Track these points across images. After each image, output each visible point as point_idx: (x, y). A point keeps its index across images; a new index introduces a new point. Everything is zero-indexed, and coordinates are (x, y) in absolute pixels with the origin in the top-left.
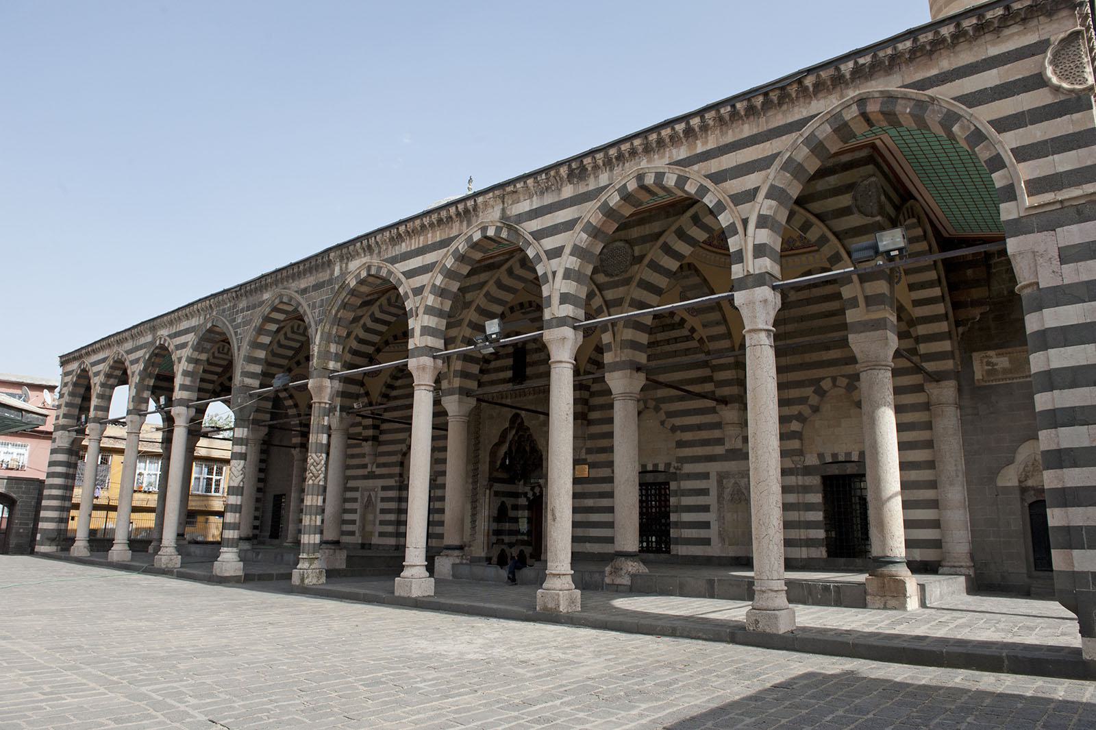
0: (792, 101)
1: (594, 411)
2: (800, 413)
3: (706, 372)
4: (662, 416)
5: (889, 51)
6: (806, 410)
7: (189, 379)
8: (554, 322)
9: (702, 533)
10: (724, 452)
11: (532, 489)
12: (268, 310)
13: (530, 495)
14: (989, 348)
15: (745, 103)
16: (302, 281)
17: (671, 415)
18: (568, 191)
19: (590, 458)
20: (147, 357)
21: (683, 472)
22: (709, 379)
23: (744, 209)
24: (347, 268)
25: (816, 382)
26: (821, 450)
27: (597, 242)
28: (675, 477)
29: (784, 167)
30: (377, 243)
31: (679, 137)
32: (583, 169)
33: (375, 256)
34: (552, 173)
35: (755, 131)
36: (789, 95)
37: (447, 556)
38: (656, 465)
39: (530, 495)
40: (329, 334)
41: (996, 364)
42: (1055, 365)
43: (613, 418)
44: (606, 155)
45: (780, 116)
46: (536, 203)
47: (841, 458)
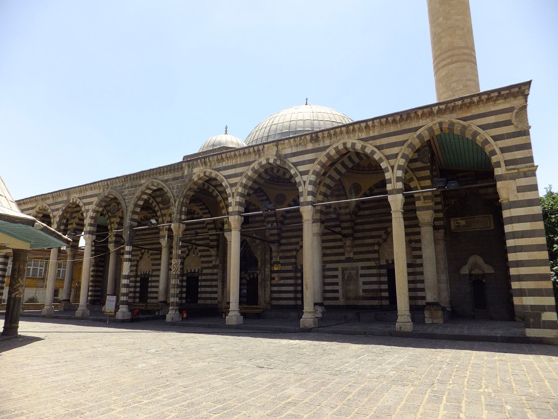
0: (411, 119)
2: (378, 242)
3: (338, 223)
5: (452, 104)
6: (381, 241)
8: (305, 203)
11: (249, 275)
12: (144, 188)
13: (248, 278)
14: (458, 217)
15: (392, 118)
16: (165, 176)
18: (310, 146)
19: (282, 261)
20: (64, 208)
22: (339, 226)
23: (392, 162)
24: (192, 171)
26: (387, 258)
29: (409, 146)
30: (210, 161)
31: (362, 129)
32: (317, 137)
33: (208, 166)
34: (303, 138)
35: (395, 130)
36: (411, 117)
39: (248, 278)
40: (182, 202)
42: (515, 230)
44: (329, 133)
45: (406, 125)
46: (294, 150)
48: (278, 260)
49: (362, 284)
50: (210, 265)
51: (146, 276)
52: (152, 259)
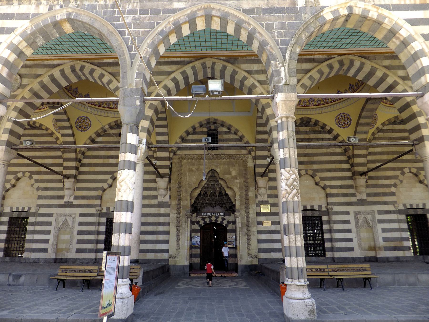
4: (33, 181)
6: (105, 186)
11: (203, 219)
13: (202, 223)
21: (333, 210)
22: (61, 165)
25: (401, 169)
26: (405, 203)
39: (202, 223)
48: (266, 199)
50: (62, 202)
51: (23, 215)
52: (38, 189)
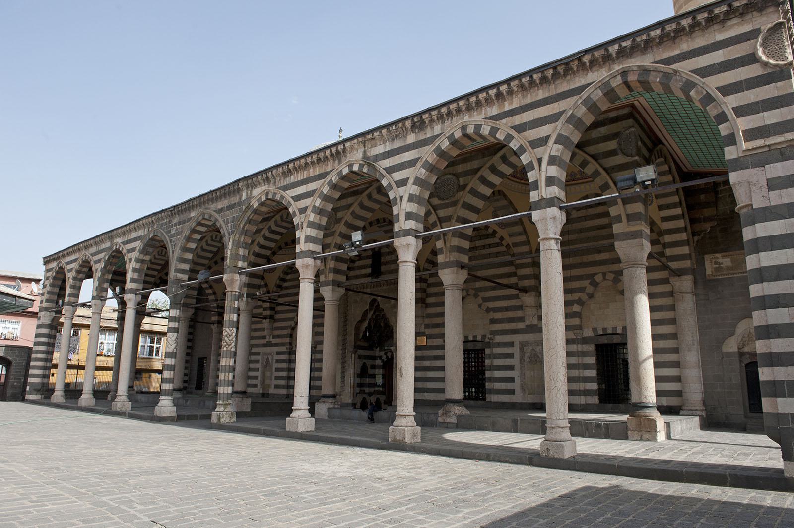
0: (574, 73)
1: (430, 297)
2: (580, 299)
3: (511, 269)
4: (480, 301)
5: (644, 37)
6: (584, 297)
7: (137, 274)
8: (402, 233)
9: (509, 386)
10: (525, 327)
11: (386, 354)
12: (194, 224)
13: (384, 358)
14: (717, 252)
15: (540, 75)
16: (219, 203)
17: (486, 300)
18: (411, 138)
19: (428, 331)
20: (106, 258)
21: (495, 341)
22: (514, 274)
23: (539, 151)
24: (251, 194)
25: (591, 277)
26: (595, 326)
27: (433, 175)
28: (489, 345)
29: (568, 121)
30: (273, 176)
31: (492, 99)
32: (422, 122)
33: (271, 185)
34: (400, 125)
35: (547, 95)
36: (572, 69)
37: (324, 402)
38: (475, 337)
39: (384, 358)
40: (239, 241)
41: (722, 263)
42: (764, 264)
43: (444, 302)
44: (439, 112)
45: (565, 84)
46: (388, 147)
47: (609, 331)
49: (260, 369)
